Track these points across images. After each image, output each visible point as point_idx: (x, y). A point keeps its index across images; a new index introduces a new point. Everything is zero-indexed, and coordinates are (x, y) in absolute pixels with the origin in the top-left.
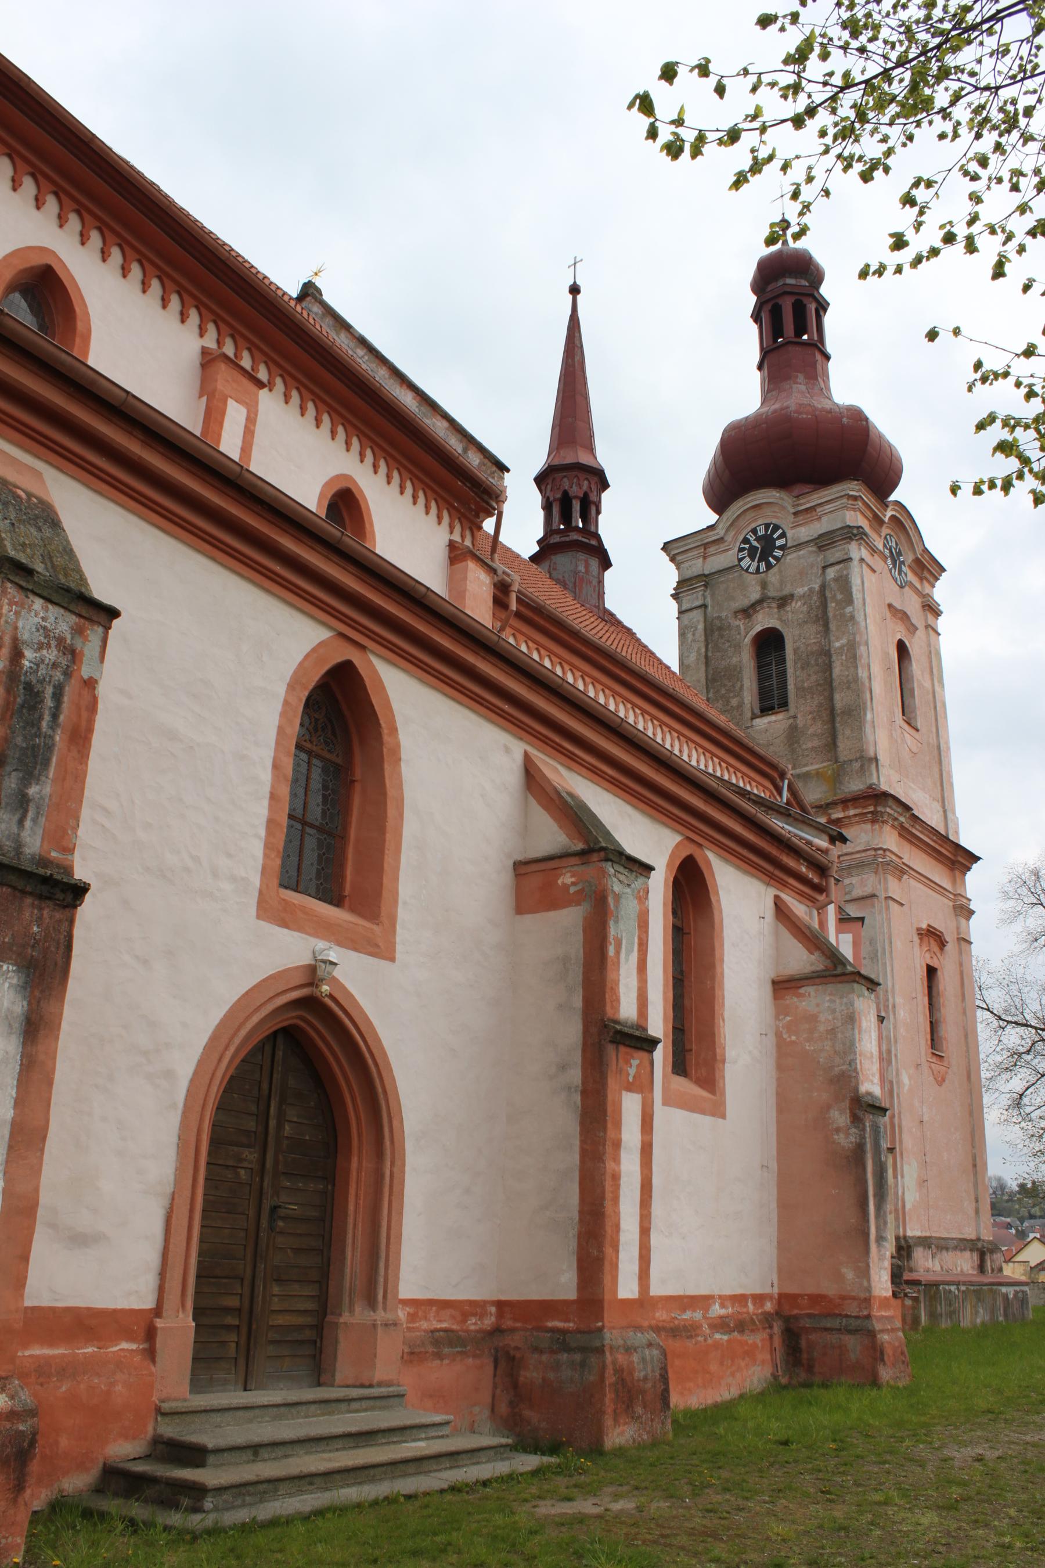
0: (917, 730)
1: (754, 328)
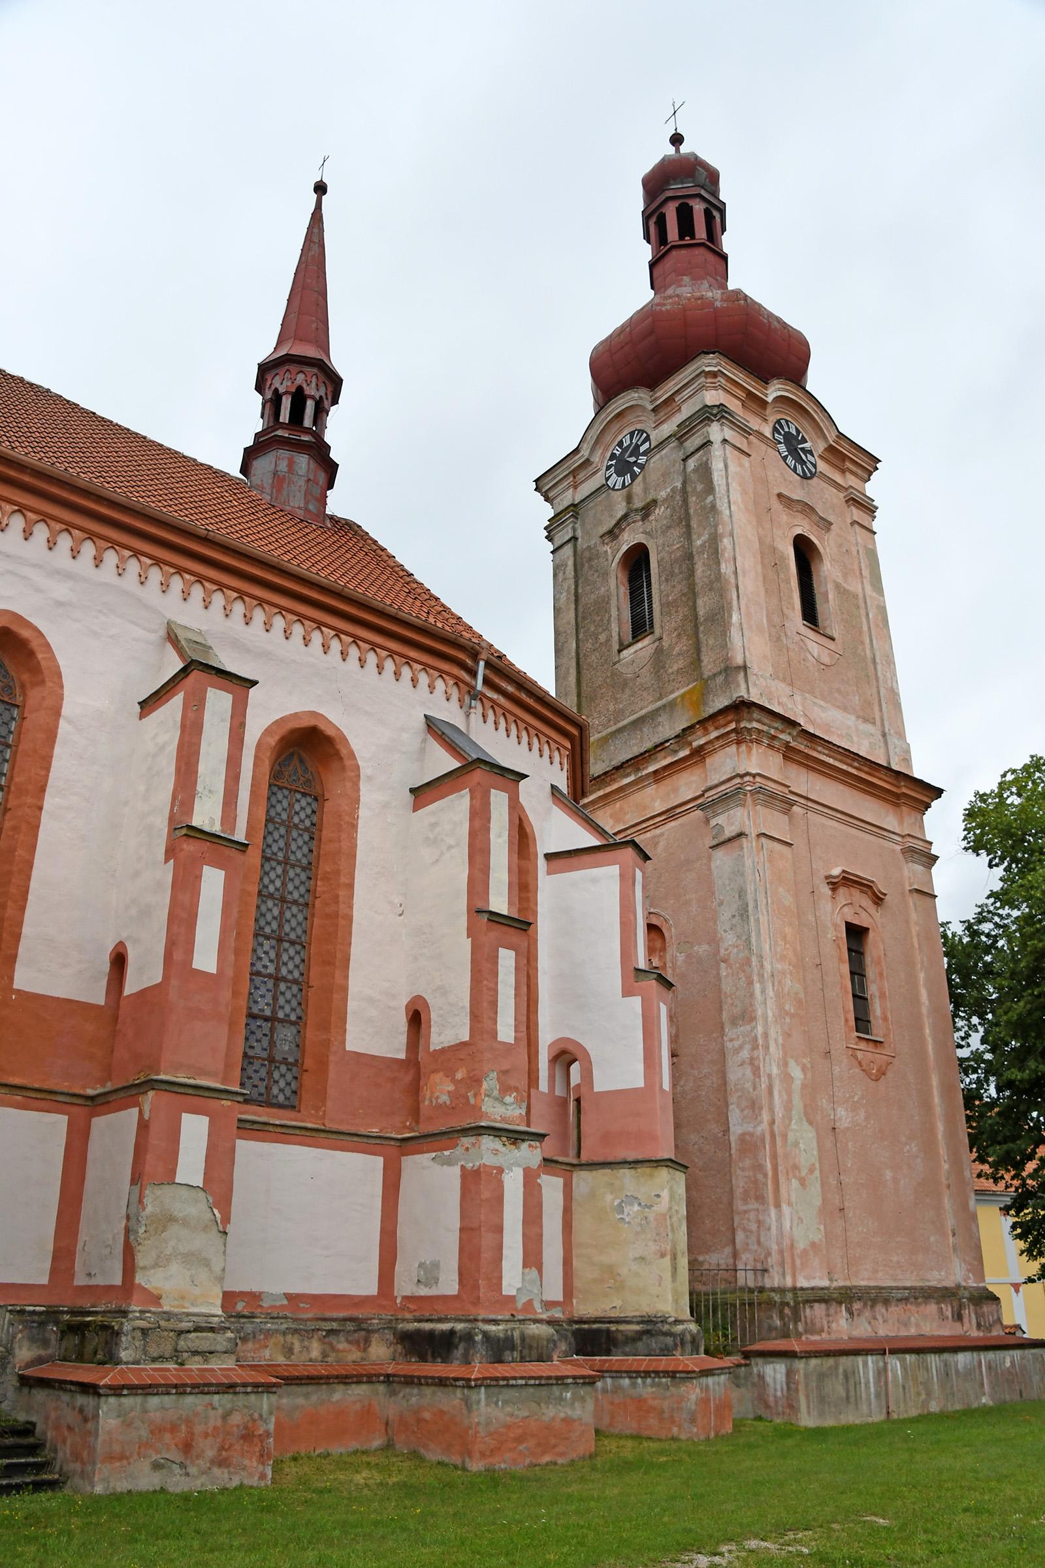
0: (833, 639)
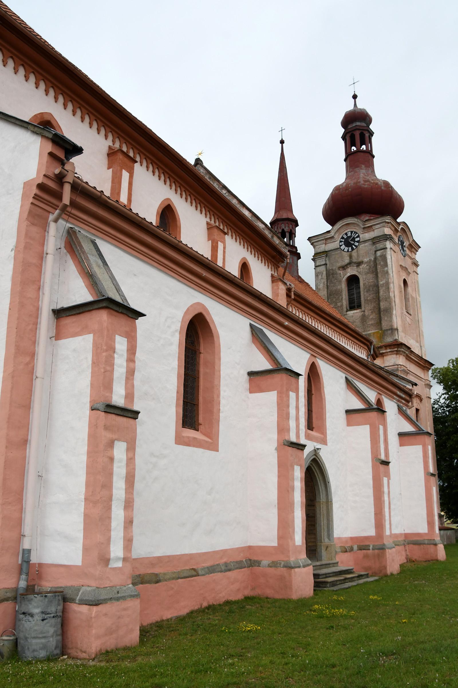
1: (342, 143)
